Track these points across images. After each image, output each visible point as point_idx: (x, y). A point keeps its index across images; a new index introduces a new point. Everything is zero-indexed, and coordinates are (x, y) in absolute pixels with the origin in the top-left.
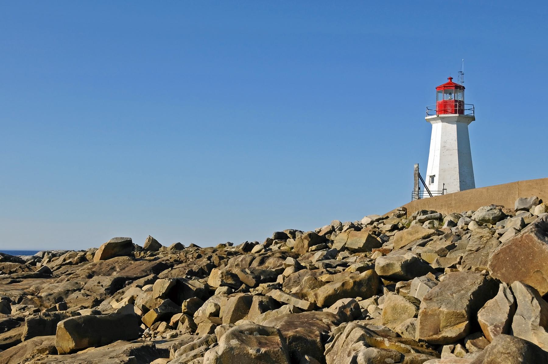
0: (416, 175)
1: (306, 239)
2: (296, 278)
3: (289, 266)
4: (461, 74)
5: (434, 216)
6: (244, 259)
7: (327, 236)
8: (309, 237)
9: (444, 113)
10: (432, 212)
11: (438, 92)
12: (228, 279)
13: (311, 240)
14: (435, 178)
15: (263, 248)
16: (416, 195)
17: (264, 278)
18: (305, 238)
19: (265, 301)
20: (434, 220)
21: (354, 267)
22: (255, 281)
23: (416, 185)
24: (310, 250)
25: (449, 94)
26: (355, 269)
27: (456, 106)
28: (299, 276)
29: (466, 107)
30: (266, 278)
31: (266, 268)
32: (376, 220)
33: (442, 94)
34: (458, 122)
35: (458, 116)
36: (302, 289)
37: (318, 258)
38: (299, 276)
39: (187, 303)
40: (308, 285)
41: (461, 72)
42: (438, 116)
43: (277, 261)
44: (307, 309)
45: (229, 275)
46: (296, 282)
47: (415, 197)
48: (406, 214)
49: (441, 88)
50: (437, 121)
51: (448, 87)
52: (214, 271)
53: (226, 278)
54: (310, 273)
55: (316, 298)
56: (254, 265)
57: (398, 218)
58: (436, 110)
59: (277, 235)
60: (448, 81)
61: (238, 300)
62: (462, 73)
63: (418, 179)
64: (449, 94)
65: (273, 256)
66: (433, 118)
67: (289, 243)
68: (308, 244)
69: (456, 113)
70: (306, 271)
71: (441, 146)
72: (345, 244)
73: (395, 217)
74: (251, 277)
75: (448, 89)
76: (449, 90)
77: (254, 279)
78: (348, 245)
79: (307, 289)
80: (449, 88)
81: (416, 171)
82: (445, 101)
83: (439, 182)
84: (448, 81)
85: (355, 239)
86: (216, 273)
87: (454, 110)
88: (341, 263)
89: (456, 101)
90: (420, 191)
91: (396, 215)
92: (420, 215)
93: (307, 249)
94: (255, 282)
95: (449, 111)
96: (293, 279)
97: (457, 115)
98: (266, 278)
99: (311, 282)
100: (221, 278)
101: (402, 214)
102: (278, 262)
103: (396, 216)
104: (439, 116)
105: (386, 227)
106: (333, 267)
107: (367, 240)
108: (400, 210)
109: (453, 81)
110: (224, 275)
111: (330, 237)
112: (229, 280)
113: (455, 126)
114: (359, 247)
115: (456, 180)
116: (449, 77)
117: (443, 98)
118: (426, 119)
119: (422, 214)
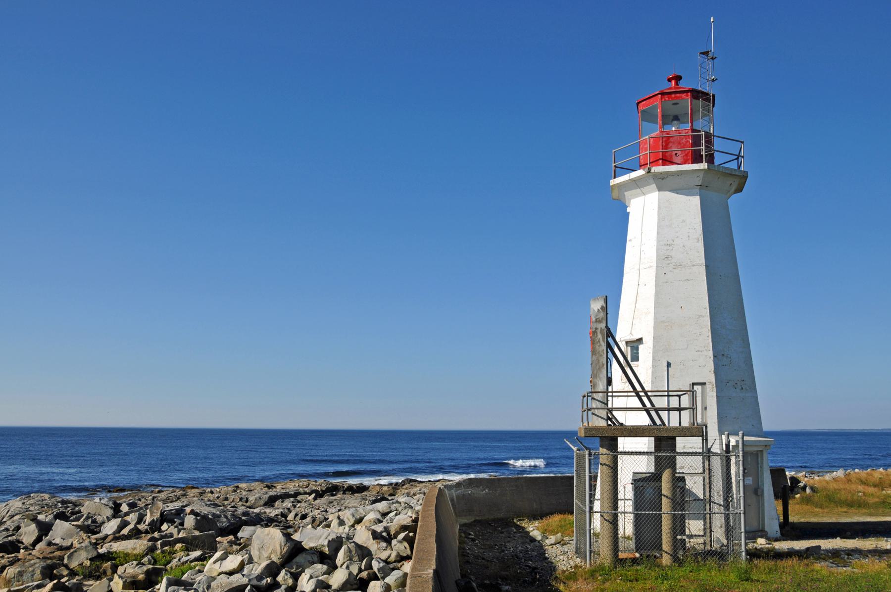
0: (600, 336)
9: (664, 165)
14: (641, 347)
23: (600, 369)
34: (703, 189)
35: (706, 167)
41: (708, 52)
42: (649, 172)
49: (652, 100)
51: (673, 95)
63: (607, 350)
66: (634, 181)
71: (658, 256)
75: (673, 99)
80: (677, 98)
81: (598, 321)
97: (704, 166)
113: (696, 201)
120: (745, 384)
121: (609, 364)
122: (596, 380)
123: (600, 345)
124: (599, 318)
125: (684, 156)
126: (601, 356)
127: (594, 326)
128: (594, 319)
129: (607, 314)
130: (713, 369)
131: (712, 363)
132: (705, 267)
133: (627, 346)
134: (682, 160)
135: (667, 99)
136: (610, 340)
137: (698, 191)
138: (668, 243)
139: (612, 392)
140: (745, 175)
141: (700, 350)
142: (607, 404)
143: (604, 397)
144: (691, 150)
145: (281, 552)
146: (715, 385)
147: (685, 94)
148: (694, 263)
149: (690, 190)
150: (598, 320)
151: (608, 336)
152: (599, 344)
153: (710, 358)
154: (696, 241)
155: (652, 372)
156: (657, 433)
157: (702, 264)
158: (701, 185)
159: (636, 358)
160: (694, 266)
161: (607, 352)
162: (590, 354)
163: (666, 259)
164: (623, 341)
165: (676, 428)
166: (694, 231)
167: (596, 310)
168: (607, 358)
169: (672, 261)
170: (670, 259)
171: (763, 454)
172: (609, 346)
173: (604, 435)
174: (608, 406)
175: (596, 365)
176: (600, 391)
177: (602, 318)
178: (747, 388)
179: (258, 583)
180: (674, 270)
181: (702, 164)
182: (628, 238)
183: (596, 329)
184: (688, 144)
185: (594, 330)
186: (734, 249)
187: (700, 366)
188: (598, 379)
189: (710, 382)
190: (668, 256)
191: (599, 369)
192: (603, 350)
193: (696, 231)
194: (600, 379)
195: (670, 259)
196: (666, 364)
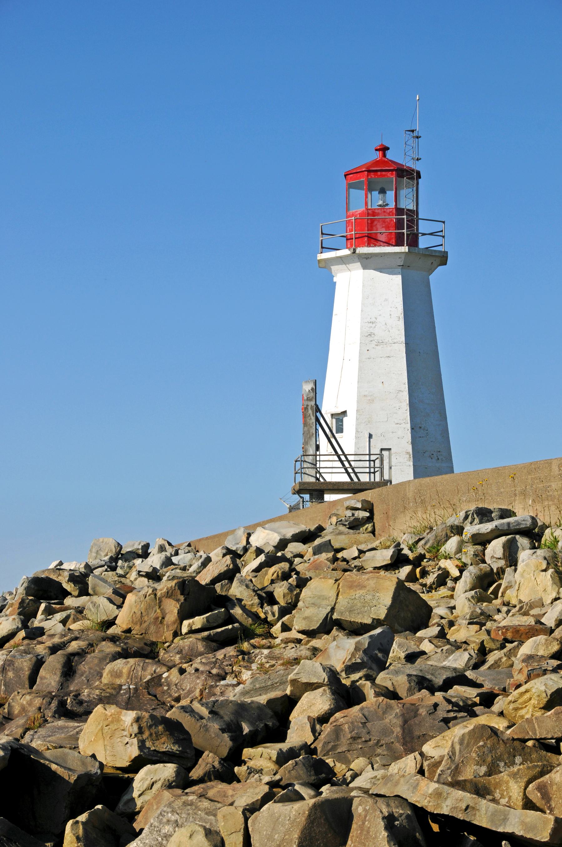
0: (310, 412)
1: (169, 597)
2: (358, 728)
3: (311, 687)
4: (413, 137)
5: (517, 525)
6: (9, 665)
7: (218, 587)
8: (179, 592)
9: (369, 245)
10: (505, 514)
11: (350, 186)
12: (158, 736)
13: (185, 600)
14: (345, 419)
15: (20, 626)
16: (309, 465)
17: (252, 729)
18: (169, 594)
19: (401, 815)
20: (518, 537)
21: (543, 688)
22: (231, 740)
23: (310, 438)
24: (184, 630)
25: (379, 193)
26: (544, 695)
27: (399, 224)
28: (364, 720)
29: (423, 227)
30: (257, 730)
31: (114, 689)
32: (293, 536)
33: (364, 192)
35: (407, 250)
36: (457, 767)
37: (350, 659)
38: (364, 720)
39: (81, 827)
40: (474, 755)
41: (413, 131)
42: (354, 252)
43: (140, 669)
44: (546, 840)
45: (161, 724)
46: (359, 741)
47: (307, 471)
48: (370, 519)
49: (359, 175)
50: (351, 266)
51: (379, 173)
52: (106, 715)
53: (151, 735)
54: (398, 711)
55: (543, 798)
56: (45, 681)
57: (352, 531)
58: (345, 234)
59: (33, 586)
60: (377, 156)
61: (309, 816)
62: (415, 134)
64: (379, 193)
65: (94, 651)
66: (341, 258)
67: (93, 609)
68: (178, 613)
69: (399, 243)
70: (384, 702)
72: (333, 609)
73: (342, 528)
74: (215, 726)
76: (381, 179)
77: (226, 735)
78: (342, 613)
79: (475, 767)
80: (382, 176)
81: (309, 399)
82: (370, 212)
83: (357, 431)
84: (377, 156)
85: (360, 597)
86: (112, 722)
87: (393, 236)
88: (454, 675)
89: (399, 211)
90: (320, 455)
91: (347, 523)
92: (471, 523)
93: (173, 628)
94: (229, 744)
95: (382, 238)
96: (347, 729)
97: (405, 249)
98: (257, 730)
99: (481, 743)
100: (136, 735)
101: (363, 518)
102: (144, 669)
103: (345, 525)
104: (357, 251)
105: (374, 557)
106: (436, 686)
107: (395, 598)
108: (357, 509)
109: (390, 155)
110: (144, 725)
111: (228, 590)
112: (162, 740)
113: (397, 280)
114: (374, 619)
115: (404, 425)
116: (377, 144)
117: (366, 204)
118: (319, 261)
119: (477, 520)
120: (442, 455)
121: (317, 434)
122: (307, 446)
123: (311, 419)
125: (388, 235)
126: (311, 427)
127: (306, 403)
128: (305, 398)
129: (316, 393)
130: (410, 441)
131: (410, 435)
132: (404, 345)
133: (332, 418)
134: (386, 238)
135: (373, 176)
136: (318, 414)
137: (400, 270)
138: (371, 320)
139: (320, 455)
140: (445, 255)
142: (316, 465)
143: (314, 460)
144: (395, 232)
145: (116, 551)
146: (412, 455)
147: (390, 172)
148: (395, 341)
149: (393, 270)
151: (316, 412)
152: (309, 418)
153: (408, 430)
154: (397, 319)
155: (355, 443)
157: (402, 342)
158: (403, 266)
159: (340, 430)
160: (395, 343)
161: (316, 424)
162: (302, 425)
164: (328, 413)
165: (368, 483)
166: (396, 310)
167: (307, 391)
168: (316, 429)
169: (375, 338)
170: (373, 336)
172: (317, 420)
174: (316, 466)
175: (307, 434)
178: (444, 459)
179: (111, 565)
180: (376, 347)
181: (403, 247)
182: (242, 844)
183: (307, 405)
184: (392, 222)
185: (306, 406)
186: (434, 326)
187: (398, 438)
189: (408, 453)
190: (371, 333)
191: (309, 437)
194: (310, 445)
195: (373, 336)
196: (368, 436)
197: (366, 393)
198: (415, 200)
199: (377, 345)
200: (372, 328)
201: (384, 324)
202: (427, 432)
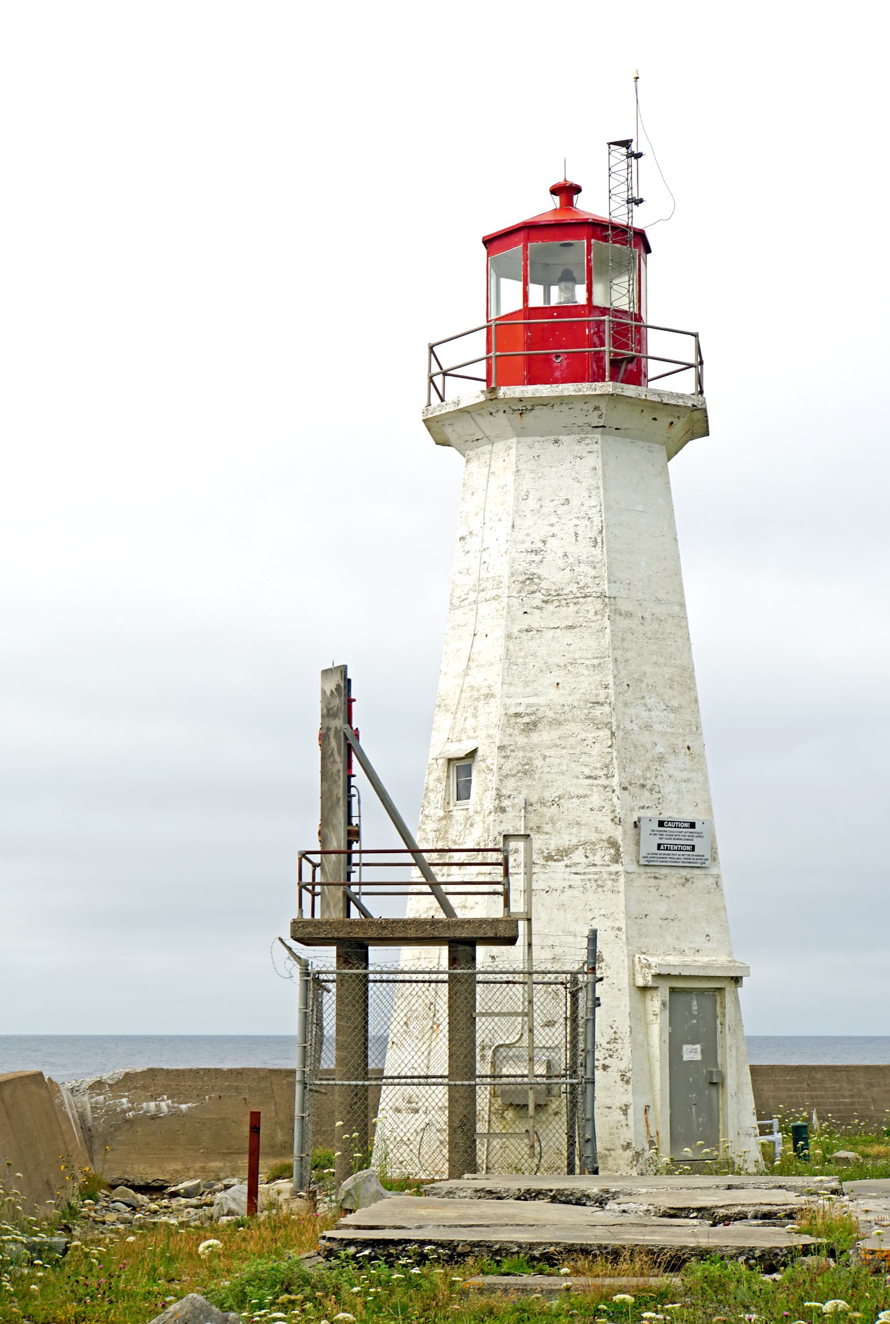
123: (334, 762)
124: (332, 708)
126: (335, 782)
141: (593, 774)
150: (331, 712)
152: (332, 760)
156: (432, 932)
163: (528, 582)
166: (588, 523)
171: (724, 996)
173: (330, 936)
176: (332, 849)
177: (338, 709)
180: (544, 605)
188: (331, 829)
190: (534, 574)
191: (331, 807)
192: (339, 771)
193: (592, 522)
197: (521, 709)
198: (636, 301)
199: (546, 602)
200: (534, 565)
201: (561, 554)
202: (660, 796)
